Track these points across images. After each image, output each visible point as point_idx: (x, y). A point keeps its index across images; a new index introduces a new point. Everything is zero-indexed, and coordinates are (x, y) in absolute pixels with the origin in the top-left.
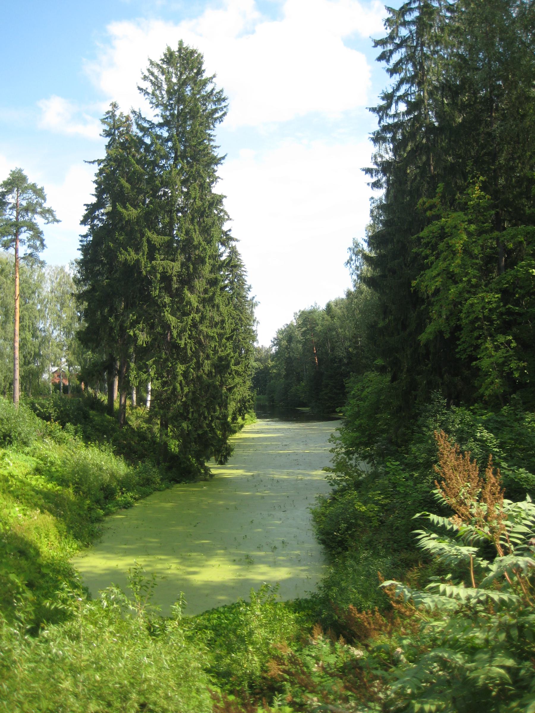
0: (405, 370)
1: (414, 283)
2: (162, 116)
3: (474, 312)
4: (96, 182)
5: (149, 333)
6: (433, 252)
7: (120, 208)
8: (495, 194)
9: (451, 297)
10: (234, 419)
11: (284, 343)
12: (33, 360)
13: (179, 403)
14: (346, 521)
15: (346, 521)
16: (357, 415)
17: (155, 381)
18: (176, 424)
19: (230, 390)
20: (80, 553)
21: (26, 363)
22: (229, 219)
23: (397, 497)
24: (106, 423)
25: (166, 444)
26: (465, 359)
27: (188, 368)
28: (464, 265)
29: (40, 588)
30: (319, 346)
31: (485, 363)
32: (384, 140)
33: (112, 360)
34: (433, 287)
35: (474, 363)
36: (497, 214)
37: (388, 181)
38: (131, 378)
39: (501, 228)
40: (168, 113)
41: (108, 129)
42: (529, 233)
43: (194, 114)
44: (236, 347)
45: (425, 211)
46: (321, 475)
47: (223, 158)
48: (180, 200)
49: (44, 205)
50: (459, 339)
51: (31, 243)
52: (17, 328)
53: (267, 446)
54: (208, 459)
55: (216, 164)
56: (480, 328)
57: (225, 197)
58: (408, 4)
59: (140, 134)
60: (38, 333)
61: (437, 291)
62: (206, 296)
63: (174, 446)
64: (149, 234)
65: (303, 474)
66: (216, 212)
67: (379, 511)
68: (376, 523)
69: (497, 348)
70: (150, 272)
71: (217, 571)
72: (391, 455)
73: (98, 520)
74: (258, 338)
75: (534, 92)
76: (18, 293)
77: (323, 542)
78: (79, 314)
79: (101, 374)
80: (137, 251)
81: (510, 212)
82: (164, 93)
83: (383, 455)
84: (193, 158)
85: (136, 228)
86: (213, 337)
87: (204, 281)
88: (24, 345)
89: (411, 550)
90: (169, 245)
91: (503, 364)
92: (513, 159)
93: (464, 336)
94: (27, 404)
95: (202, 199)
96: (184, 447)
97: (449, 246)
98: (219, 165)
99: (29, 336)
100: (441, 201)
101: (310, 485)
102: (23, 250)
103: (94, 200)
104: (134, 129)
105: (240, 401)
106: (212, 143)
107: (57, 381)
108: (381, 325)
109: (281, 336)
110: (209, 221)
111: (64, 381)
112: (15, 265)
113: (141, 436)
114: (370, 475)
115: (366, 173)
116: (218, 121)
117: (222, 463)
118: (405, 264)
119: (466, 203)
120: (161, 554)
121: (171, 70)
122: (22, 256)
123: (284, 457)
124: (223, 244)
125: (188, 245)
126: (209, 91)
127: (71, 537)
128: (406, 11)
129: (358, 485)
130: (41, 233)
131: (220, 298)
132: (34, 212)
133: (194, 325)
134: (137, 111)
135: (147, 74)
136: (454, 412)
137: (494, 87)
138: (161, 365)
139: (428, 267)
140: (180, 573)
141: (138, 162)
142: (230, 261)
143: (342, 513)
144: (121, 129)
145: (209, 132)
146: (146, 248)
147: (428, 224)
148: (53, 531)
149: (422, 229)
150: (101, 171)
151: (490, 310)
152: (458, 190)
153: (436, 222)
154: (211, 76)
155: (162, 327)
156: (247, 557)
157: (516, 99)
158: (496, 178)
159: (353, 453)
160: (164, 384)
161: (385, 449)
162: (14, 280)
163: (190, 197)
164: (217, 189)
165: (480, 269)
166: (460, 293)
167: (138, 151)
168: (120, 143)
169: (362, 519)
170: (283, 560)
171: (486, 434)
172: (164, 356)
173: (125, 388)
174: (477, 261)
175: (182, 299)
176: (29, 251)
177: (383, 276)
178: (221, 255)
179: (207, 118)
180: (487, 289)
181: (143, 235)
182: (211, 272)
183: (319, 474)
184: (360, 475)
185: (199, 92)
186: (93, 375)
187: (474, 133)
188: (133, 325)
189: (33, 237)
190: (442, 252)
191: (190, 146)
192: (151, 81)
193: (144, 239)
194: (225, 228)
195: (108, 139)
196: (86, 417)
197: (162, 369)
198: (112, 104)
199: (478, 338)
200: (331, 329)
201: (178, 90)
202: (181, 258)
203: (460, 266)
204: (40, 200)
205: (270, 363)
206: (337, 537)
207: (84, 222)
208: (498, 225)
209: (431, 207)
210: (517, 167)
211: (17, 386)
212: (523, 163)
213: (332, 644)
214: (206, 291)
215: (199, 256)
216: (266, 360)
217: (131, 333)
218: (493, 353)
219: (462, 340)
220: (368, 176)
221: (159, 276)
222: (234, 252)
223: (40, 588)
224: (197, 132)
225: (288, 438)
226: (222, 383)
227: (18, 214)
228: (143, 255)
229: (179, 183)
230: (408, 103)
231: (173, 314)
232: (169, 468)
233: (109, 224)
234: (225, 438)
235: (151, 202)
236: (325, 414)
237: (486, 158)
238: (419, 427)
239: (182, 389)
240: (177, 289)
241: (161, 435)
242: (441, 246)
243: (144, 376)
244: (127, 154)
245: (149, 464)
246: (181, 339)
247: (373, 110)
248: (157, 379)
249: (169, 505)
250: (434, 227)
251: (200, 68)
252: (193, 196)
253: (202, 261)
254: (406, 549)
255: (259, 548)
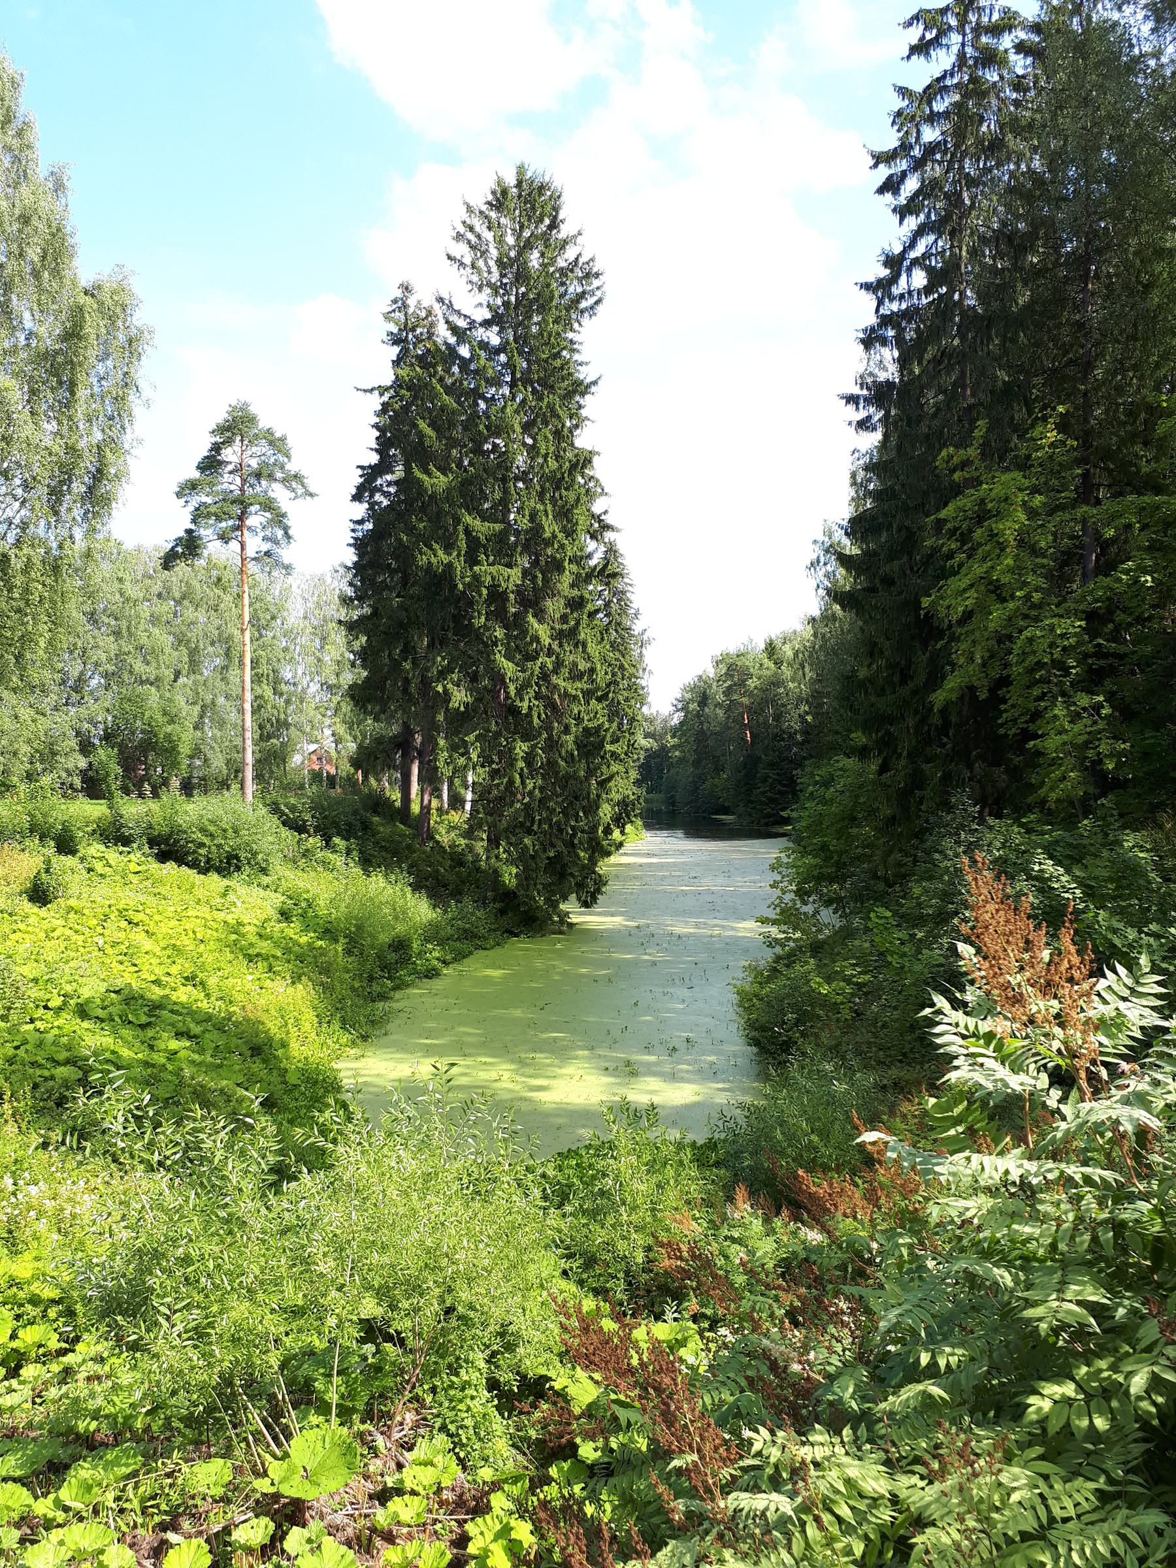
0: (905, 753)
1: (925, 602)
2: (489, 306)
3: (1034, 652)
4: (376, 426)
5: (470, 690)
6: (963, 544)
7: (418, 473)
8: (1086, 438)
9: (992, 625)
10: (608, 831)
11: (693, 706)
12: (273, 734)
13: (518, 805)
14: (796, 1008)
15: (796, 1008)
16: (816, 827)
17: (479, 770)
18: (513, 839)
19: (602, 784)
20: (353, 1052)
21: (264, 737)
22: (603, 493)
23: (885, 970)
24: (397, 838)
25: (496, 873)
26: (1015, 735)
27: (534, 747)
28: (1020, 568)
29: (286, 1109)
30: (753, 711)
31: (1052, 744)
32: (884, 342)
33: (407, 732)
34: (960, 609)
35: (1032, 743)
36: (1085, 475)
37: (885, 420)
38: (440, 764)
39: (1093, 501)
40: (499, 301)
41: (395, 331)
42: (1144, 509)
43: (543, 303)
44: (614, 713)
45: (953, 471)
46: (751, 930)
47: (595, 383)
48: (521, 461)
49: (287, 467)
50: (1005, 701)
51: (268, 533)
52: (248, 679)
53: (663, 878)
54: (565, 898)
55: (583, 394)
56: (1042, 681)
57: (598, 454)
58: (938, 80)
59: (452, 340)
60: (283, 687)
61: (968, 615)
62: (565, 627)
63: (509, 875)
64: (468, 519)
65: (723, 927)
66: (582, 481)
67: (853, 995)
68: (846, 1014)
69: (1075, 717)
70: (468, 586)
71: (577, 1086)
72: (876, 900)
73: (383, 997)
74: (649, 699)
75: (1174, 240)
76: (247, 619)
77: (754, 1042)
78: (352, 657)
79: (389, 756)
80: (448, 548)
81: (1110, 471)
82: (492, 263)
83: (863, 899)
84: (543, 382)
85: (446, 507)
86: (575, 697)
87: (562, 601)
88: (260, 707)
89: (909, 1064)
90: (501, 537)
91: (1086, 745)
92: (1123, 370)
93: (1014, 695)
94: (265, 805)
95: (557, 458)
96: (526, 878)
97: (993, 535)
98: (587, 397)
99: (268, 692)
100: (982, 454)
101: (732, 945)
102: (255, 544)
103: (374, 458)
104: (443, 333)
105: (618, 803)
106: (576, 357)
107: (317, 768)
108: (863, 673)
109: (688, 696)
110: (571, 496)
111: (328, 767)
112: (242, 571)
113: (457, 859)
114: (836, 933)
115: (848, 402)
116: (586, 315)
117: (587, 903)
118: (912, 569)
119: (1028, 457)
120: (485, 1055)
121: (503, 220)
122: (254, 555)
123: (694, 902)
124: (593, 537)
125: (534, 539)
126: (572, 259)
127: (336, 1025)
128: (935, 95)
129: (816, 948)
130: (284, 515)
131: (588, 631)
132: (271, 477)
133: (545, 676)
134: (445, 296)
135: (462, 229)
136: (991, 828)
137: (1093, 235)
138: (489, 743)
139: (954, 573)
140: (518, 1088)
141: (449, 390)
142: (606, 566)
143: (788, 995)
144: (419, 331)
145: (570, 335)
146: (463, 545)
147: (957, 495)
148: (309, 1018)
149: (946, 505)
150: (385, 407)
151: (1064, 649)
152: (1015, 431)
153: (972, 491)
154: (574, 232)
155: (492, 679)
156: (628, 1063)
157: (1135, 254)
158: (1087, 408)
159: (809, 894)
160: (494, 774)
161: (866, 888)
162: (239, 596)
163: (538, 453)
164: (583, 440)
165: (1048, 576)
166: (1010, 619)
167: (447, 371)
168: (417, 356)
169: (823, 1006)
170: (687, 1071)
171: (1049, 866)
172: (494, 728)
173: (430, 779)
174: (1045, 561)
175: (524, 632)
176: (265, 547)
177: (871, 590)
178: (590, 556)
179: (568, 309)
180: (1061, 611)
181: (457, 520)
182: (572, 586)
183: (748, 928)
184: (820, 931)
185: (553, 260)
186: (376, 758)
187: (1050, 323)
188: (443, 674)
189: (272, 523)
190: (980, 545)
191: (538, 361)
192: (469, 242)
193: (461, 528)
194: (597, 507)
195: (396, 350)
196: (366, 826)
197: (491, 748)
198: (402, 285)
199: (1041, 698)
200: (776, 682)
201: (517, 259)
202: (524, 562)
203: (1010, 570)
204: (282, 458)
205: (671, 741)
206: (776, 1032)
207: (357, 498)
208: (1087, 493)
209: (965, 464)
210: (1130, 385)
211: (249, 773)
212: (1141, 378)
213: (767, 1220)
214: (564, 619)
215: (553, 558)
216: (662, 736)
217: (440, 689)
218: (1067, 726)
219: (1010, 702)
220: (851, 407)
221: (485, 592)
222: (611, 551)
223: (284, 1109)
224: (550, 335)
225: (698, 865)
226: (591, 772)
227: (244, 481)
228: (459, 555)
229: (518, 429)
230: (930, 271)
231: (509, 657)
232: (502, 912)
233: (400, 502)
234: (593, 862)
235: (471, 464)
236: (761, 826)
237: (1071, 371)
238: (928, 853)
239: (523, 783)
240: (515, 614)
241: (488, 858)
242: (979, 534)
243: (462, 761)
244: (430, 376)
245: (468, 905)
246: (522, 700)
247: (867, 287)
248: (483, 766)
249: (496, 973)
250: (967, 501)
251: (555, 217)
252: (543, 452)
253: (559, 567)
254: (901, 1061)
255: (648, 1049)
